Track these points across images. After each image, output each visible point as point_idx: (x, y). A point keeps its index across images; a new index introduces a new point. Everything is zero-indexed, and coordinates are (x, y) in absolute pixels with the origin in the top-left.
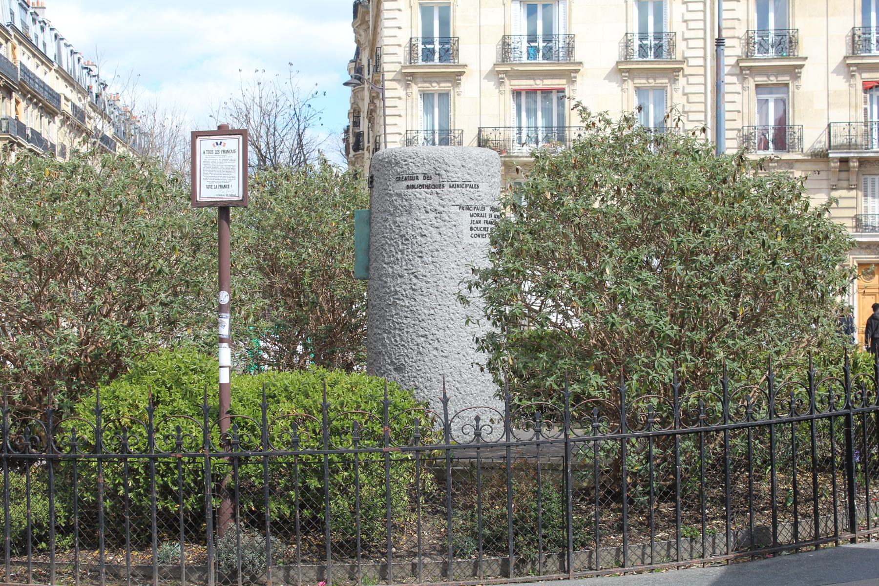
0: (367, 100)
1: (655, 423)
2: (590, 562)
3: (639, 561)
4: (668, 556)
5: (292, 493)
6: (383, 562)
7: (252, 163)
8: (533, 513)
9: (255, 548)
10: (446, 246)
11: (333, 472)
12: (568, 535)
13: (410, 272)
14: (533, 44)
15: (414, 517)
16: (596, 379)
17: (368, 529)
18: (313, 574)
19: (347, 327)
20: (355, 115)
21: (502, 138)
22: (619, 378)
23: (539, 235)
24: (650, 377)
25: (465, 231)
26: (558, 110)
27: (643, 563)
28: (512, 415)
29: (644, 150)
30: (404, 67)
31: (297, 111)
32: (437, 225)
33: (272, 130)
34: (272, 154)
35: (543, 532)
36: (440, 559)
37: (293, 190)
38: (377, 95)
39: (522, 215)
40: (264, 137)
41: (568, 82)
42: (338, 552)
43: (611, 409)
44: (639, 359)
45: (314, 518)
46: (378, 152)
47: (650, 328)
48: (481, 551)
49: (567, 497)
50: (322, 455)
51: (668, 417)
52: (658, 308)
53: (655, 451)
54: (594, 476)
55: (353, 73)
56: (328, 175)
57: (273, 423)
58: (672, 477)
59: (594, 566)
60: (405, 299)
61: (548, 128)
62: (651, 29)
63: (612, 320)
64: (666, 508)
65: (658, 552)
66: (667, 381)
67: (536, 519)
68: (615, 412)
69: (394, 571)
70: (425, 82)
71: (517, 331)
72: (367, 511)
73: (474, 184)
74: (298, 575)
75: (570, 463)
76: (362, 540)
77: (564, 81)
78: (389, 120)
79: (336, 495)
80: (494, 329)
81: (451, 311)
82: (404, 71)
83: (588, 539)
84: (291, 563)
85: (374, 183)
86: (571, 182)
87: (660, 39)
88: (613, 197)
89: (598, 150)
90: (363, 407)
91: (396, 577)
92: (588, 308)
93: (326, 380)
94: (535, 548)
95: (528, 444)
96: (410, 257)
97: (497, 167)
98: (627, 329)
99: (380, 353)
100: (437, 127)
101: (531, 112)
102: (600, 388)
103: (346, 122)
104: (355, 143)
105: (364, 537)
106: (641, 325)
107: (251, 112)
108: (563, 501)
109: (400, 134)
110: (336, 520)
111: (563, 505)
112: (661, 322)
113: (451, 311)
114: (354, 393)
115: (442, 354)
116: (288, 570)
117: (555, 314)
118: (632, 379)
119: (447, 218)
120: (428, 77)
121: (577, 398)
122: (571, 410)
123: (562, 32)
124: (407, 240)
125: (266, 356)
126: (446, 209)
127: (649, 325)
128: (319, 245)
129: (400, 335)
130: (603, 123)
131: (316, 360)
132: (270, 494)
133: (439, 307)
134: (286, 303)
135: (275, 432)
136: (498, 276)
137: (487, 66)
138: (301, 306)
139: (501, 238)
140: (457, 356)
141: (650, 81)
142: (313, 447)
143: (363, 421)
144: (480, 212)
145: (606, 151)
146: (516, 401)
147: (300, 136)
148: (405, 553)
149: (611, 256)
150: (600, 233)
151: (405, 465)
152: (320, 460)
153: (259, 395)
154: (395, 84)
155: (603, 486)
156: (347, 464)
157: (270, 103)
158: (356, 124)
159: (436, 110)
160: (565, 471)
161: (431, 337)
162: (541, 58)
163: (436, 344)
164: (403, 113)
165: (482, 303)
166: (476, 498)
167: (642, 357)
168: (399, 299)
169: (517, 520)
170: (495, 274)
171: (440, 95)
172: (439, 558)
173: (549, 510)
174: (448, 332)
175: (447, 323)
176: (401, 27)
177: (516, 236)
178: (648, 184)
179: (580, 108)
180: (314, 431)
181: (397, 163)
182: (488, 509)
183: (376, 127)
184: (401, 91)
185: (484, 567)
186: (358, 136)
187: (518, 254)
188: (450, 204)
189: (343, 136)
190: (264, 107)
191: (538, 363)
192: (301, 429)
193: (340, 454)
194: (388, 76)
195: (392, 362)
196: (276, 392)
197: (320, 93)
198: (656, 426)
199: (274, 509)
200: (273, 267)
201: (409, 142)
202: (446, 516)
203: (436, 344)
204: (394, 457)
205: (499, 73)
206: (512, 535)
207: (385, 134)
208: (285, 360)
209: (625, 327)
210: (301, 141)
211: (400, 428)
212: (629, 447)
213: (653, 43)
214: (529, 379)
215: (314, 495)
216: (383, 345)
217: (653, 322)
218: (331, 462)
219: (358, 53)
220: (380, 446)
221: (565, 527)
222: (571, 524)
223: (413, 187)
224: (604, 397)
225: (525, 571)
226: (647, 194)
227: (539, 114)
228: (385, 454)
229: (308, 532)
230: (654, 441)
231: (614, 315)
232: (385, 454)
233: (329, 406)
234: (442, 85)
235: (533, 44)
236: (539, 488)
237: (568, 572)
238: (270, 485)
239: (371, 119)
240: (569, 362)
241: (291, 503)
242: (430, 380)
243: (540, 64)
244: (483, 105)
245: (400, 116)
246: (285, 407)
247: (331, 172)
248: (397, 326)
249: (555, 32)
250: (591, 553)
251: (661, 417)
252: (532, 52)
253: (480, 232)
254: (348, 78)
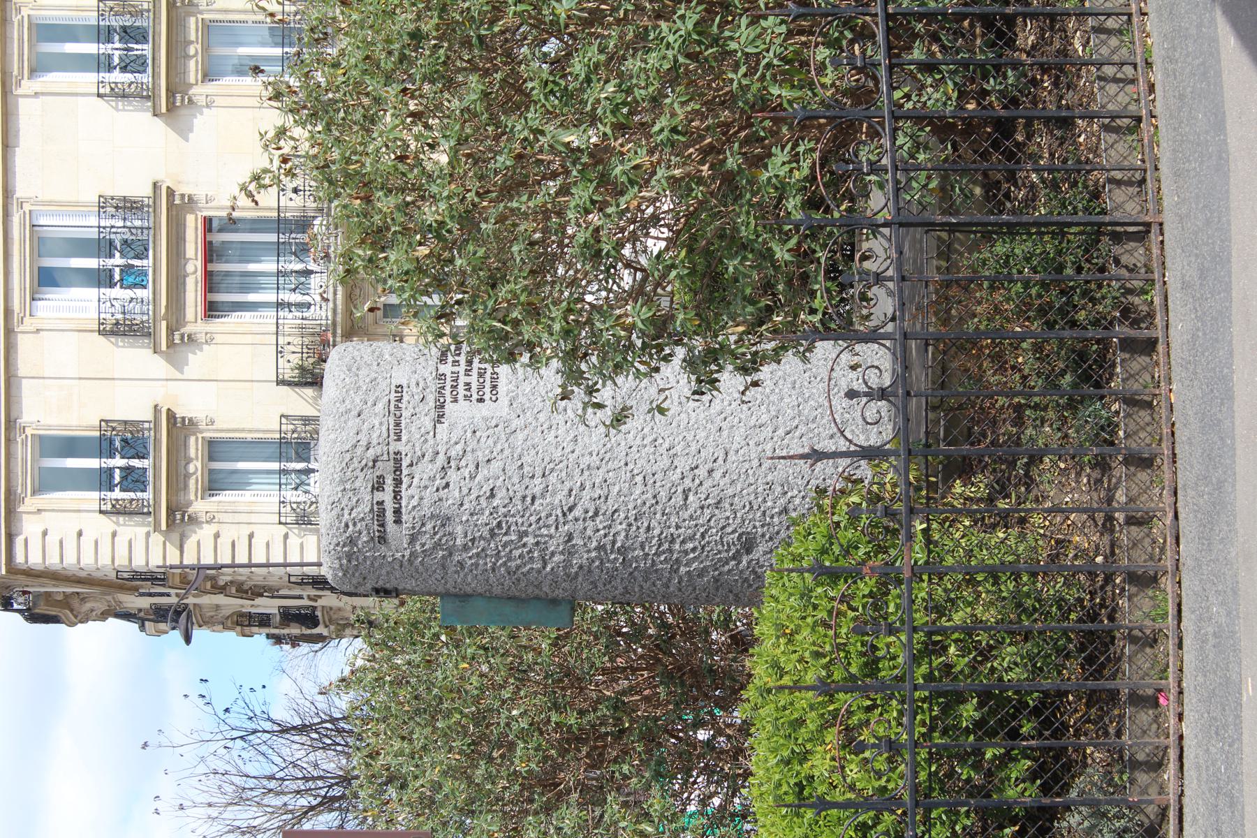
0: (220, 599)
1: (863, 53)
2: (1130, 183)
3: (1130, 88)
4: (1120, 32)
5: (988, 755)
6: (1124, 581)
7: (336, 823)
8: (1034, 291)
9: (1093, 827)
10: (513, 449)
11: (948, 674)
12: (1077, 224)
13: (561, 520)
14: (117, 277)
15: (1036, 519)
16: (778, 163)
17: (1060, 608)
18: (1145, 717)
19: (663, 645)
20: (246, 623)
21: (298, 340)
22: (776, 121)
23: (498, 269)
24: (775, 62)
25: (485, 413)
26: (244, 231)
27: (1133, 81)
28: (841, 328)
29: (336, 65)
30: (157, 528)
31: (236, 734)
32: (472, 467)
33: (273, 784)
34: (320, 783)
35: (1069, 271)
36: (1119, 471)
37: (397, 744)
38: (207, 578)
39: (459, 302)
40: (286, 799)
41: (192, 211)
42: (1103, 666)
43: (835, 137)
44: (740, 83)
45: (1036, 711)
46: (330, 578)
47: (681, 59)
48: (1105, 391)
49: (1001, 225)
50: (917, 694)
51: (852, 30)
52: (641, 43)
53: (917, 54)
54: (964, 172)
55: (162, 626)
56: (371, 676)
57: (852, 787)
58: (966, 23)
59: (1138, 176)
60: (613, 531)
61: (279, 250)
62: (91, 48)
63: (666, 133)
64: (1027, 36)
65: (1113, 52)
66: (783, 29)
67: (1044, 285)
68: (842, 130)
69: (1140, 560)
70: (186, 487)
71: (681, 316)
72: (1025, 610)
74: (1145, 744)
75: (939, 219)
76: (1080, 620)
77: (190, 219)
78: (259, 558)
79: (993, 669)
80: (677, 361)
81: (638, 441)
82: (164, 527)
83: (1086, 187)
84: (1121, 757)
85: (388, 586)
86: (398, 207)
87: (110, 30)
88: (426, 126)
89: (336, 154)
90: (824, 615)
91: (1151, 558)
92: (640, 177)
93: (771, 684)
94: (1100, 287)
95: (901, 298)
96: (533, 519)
97: (358, 349)
98: (683, 104)
99: (716, 581)
100: (275, 466)
101: (249, 282)
102: (795, 158)
103: (259, 640)
104: (300, 624)
105: (1073, 616)
106: (673, 76)
107: (237, 823)
108: (1010, 233)
109: (286, 537)
110: (1041, 669)
111: (1018, 233)
112: (671, 39)
113: (638, 441)
114: (797, 631)
115: (720, 461)
116: (1135, 765)
117: (650, 242)
118: (779, 96)
119: (459, 447)
120: (177, 480)
121: (813, 203)
122: (836, 215)
123: (93, 221)
124: (499, 525)
125: (716, 801)
126: (442, 449)
127: (676, 61)
128: (506, 694)
129: (683, 542)
130: (282, 143)
131: (727, 704)
132: (988, 796)
133: (631, 466)
134: (615, 761)
135: (869, 786)
136: (575, 350)
137: (156, 365)
138: (622, 731)
139: (506, 346)
140: (725, 433)
141: (192, 51)
142: (901, 713)
143: (851, 614)
144: (449, 383)
145: (337, 140)
146: (816, 318)
147: (285, 730)
148: (1106, 539)
149: (542, 133)
150: (496, 153)
151: (936, 537)
152: (924, 701)
153: (798, 815)
154: (190, 545)
155: (985, 156)
156: (934, 648)
157: (220, 787)
158: (263, 621)
159: (241, 465)
160: (952, 228)
161: (688, 482)
162: (145, 262)
163: (702, 472)
164: (246, 531)
165: (626, 382)
166: (1002, 401)
167: (736, 77)
168: (614, 542)
169: (1047, 323)
170: (573, 356)
171: (211, 458)
172: (1116, 473)
173: (1028, 260)
174: (678, 449)
175: (662, 450)
176: (70, 530)
177: (500, 315)
178: (403, 58)
179: (252, 187)
180: (869, 709)
181: (352, 541)
182: (1024, 378)
183: (273, 582)
184: (204, 534)
185: (1136, 386)
186: (289, 616)
187: (534, 312)
188: (431, 442)
189: (287, 647)
190: (228, 799)
191: (745, 276)
192: (865, 736)
193: (915, 660)
194: (173, 558)
195: (734, 558)
196: (792, 782)
197: (203, 689)
198: (869, 53)
199: (1018, 789)
200: (546, 787)
201: (304, 519)
202: (1035, 459)
203: (702, 472)
204: (921, 557)
205: (171, 344)
206: (1076, 333)
207: (285, 565)
208: (729, 762)
209: (677, 108)
210: (294, 728)
211: (864, 543)
212: (909, 105)
213: (117, 45)
214: (774, 295)
215: (992, 712)
216: (702, 573)
217: (670, 53)
218: (929, 677)
219: (127, 616)
220: (899, 582)
221: (1060, 230)
222: (1056, 218)
223: (397, 512)
224: (813, 150)
225: (1145, 308)
226: (422, 62)
227: (252, 267)
228: (916, 574)
229: (1062, 723)
230: (898, 56)
231: (656, 128)
232: (916, 574)
233: (820, 679)
234: (192, 453)
235: (117, 277)
236: (987, 278)
237: (1148, 225)
238: (970, 795)
239: (256, 592)
240: (743, 217)
241: (1006, 759)
242: (770, 485)
243: (156, 262)
244: (233, 377)
245: (251, 536)
246: (820, 764)
247: (364, 669)
248: (666, 546)
249: (93, 234)
250: (1111, 181)
251: (852, 42)
252: (131, 279)
253: (488, 385)
254: (176, 635)
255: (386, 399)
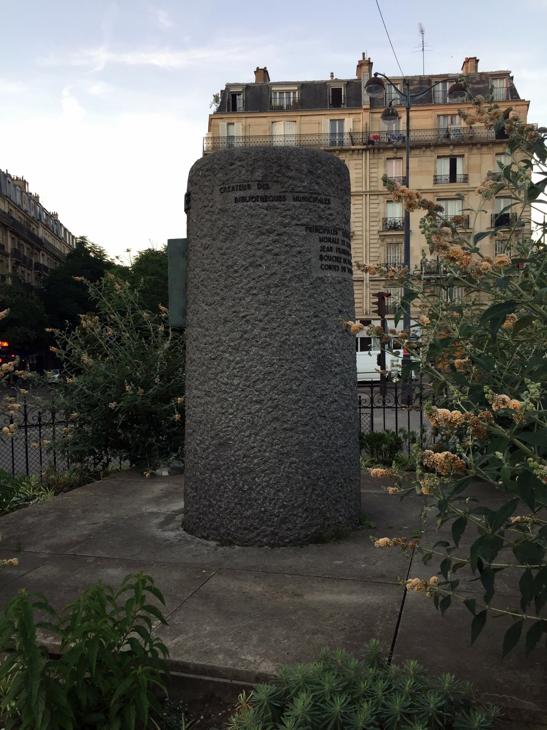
25: (314, 260)
73: (324, 197)
85: (192, 201)
255: (320, 191)
